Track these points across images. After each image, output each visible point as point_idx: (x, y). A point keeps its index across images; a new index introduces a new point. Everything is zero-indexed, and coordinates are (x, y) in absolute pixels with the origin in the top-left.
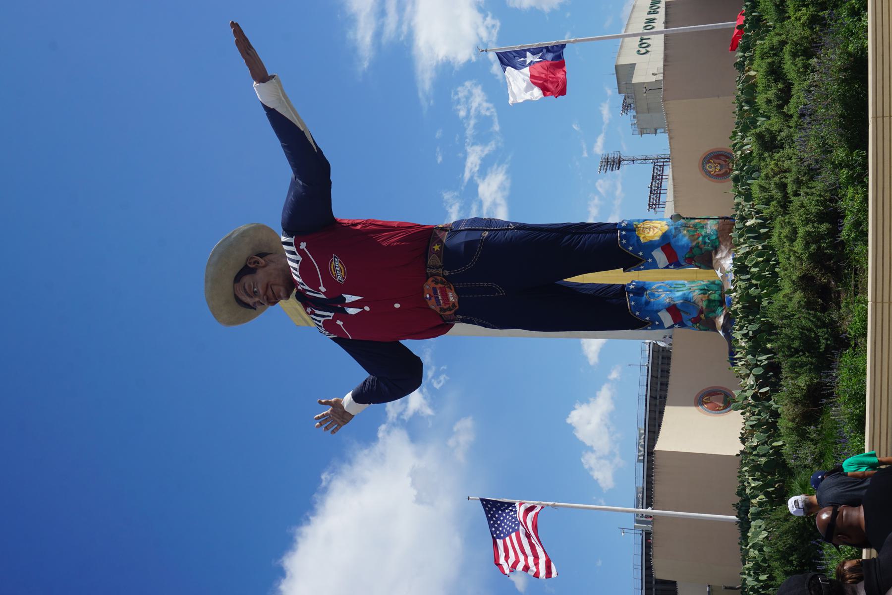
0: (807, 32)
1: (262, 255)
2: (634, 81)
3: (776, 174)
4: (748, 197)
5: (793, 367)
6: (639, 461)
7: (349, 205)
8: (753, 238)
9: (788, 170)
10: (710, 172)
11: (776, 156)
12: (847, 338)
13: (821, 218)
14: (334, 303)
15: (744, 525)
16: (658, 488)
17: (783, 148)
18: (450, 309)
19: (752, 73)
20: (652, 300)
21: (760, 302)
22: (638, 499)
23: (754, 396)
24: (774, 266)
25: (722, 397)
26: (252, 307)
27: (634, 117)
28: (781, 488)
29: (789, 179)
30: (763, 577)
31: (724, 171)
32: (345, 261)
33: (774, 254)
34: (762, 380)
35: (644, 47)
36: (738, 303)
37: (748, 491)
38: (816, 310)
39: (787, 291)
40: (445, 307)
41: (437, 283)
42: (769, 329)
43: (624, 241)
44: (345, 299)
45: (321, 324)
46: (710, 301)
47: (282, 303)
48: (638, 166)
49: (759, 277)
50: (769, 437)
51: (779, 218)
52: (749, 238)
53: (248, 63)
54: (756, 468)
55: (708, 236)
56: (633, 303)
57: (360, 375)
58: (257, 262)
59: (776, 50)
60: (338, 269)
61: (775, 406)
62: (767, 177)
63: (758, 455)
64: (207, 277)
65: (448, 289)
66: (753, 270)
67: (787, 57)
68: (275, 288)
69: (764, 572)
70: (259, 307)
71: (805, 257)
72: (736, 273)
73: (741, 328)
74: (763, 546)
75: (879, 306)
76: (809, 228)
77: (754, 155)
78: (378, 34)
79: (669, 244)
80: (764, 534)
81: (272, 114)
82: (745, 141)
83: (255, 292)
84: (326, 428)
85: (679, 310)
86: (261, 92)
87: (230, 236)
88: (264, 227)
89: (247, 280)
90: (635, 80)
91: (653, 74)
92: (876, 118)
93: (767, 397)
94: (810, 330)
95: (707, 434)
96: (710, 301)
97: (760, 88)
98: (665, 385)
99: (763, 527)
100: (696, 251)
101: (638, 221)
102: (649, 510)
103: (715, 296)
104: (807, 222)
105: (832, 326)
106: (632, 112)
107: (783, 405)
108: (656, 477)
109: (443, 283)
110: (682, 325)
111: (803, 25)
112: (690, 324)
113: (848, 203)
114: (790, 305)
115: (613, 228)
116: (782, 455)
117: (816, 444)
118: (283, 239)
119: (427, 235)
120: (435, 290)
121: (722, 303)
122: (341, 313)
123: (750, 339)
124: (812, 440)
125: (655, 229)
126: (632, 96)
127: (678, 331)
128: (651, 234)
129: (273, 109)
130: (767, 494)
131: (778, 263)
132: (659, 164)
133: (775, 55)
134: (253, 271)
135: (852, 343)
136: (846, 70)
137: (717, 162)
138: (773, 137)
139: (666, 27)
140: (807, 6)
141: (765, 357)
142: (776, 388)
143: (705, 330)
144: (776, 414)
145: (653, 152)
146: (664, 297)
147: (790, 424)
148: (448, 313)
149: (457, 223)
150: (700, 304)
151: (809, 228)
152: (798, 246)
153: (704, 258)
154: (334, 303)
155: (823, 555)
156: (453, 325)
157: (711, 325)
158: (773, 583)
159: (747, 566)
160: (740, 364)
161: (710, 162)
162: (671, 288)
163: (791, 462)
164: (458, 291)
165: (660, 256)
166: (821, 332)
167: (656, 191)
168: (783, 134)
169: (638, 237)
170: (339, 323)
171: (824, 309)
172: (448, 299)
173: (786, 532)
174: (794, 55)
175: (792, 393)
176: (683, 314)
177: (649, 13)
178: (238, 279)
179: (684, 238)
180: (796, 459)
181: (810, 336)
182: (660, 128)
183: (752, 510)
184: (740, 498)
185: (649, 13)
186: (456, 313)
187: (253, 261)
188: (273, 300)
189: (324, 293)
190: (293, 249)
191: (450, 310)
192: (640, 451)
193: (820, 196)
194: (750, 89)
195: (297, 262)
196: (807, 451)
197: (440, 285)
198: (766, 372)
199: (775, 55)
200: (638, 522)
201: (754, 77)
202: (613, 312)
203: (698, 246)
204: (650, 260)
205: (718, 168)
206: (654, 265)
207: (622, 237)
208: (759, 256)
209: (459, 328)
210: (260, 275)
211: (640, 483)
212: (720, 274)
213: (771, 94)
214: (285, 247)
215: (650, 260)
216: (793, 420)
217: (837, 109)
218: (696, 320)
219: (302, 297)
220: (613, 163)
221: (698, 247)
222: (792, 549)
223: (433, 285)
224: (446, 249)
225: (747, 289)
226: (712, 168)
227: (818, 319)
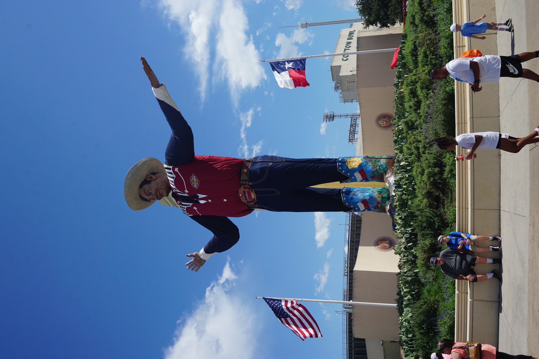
0: (428, 77)
1: (154, 174)
3: (414, 142)
4: (401, 152)
5: (423, 235)
6: (345, 275)
7: (202, 149)
8: (404, 171)
9: (420, 141)
11: (415, 133)
12: (447, 223)
13: (436, 165)
14: (193, 198)
15: (400, 311)
16: (355, 290)
17: (417, 129)
18: (252, 202)
19: (402, 90)
21: (407, 202)
22: (344, 295)
23: (405, 248)
24: (414, 185)
25: (388, 241)
26: (146, 200)
27: (341, 93)
28: (418, 292)
29: (421, 145)
30: (410, 336)
32: (198, 177)
33: (414, 179)
34: (408, 240)
36: (397, 202)
37: (402, 293)
38: (433, 208)
39: (420, 198)
41: (245, 189)
42: (412, 216)
46: (383, 197)
48: (343, 119)
49: (407, 190)
50: (412, 268)
51: (416, 164)
52: (402, 171)
53: (150, 78)
54: (406, 282)
55: (381, 166)
57: (208, 235)
59: (414, 83)
60: (195, 181)
61: (415, 252)
62: (410, 143)
63: (407, 276)
66: (404, 187)
67: (419, 89)
68: (161, 191)
69: (410, 333)
70: (152, 201)
71: (428, 183)
72: (396, 187)
73: (399, 215)
74: (410, 320)
75: (461, 209)
76: (430, 170)
77: (404, 131)
79: (362, 170)
80: (410, 315)
81: (162, 104)
82: (400, 123)
83: (150, 193)
84: (193, 269)
85: (367, 202)
88: (155, 159)
89: (146, 187)
92: (458, 123)
93: (411, 248)
94: (431, 218)
95: (379, 261)
96: (383, 197)
97: (406, 100)
98: (359, 235)
99: (410, 311)
100: (376, 173)
101: (347, 158)
102: (351, 301)
103: (385, 195)
104: (429, 167)
105: (441, 217)
107: (418, 251)
108: (355, 284)
109: (248, 188)
110: (369, 210)
111: (426, 74)
112: (373, 209)
113: (447, 159)
114: (422, 205)
115: (335, 161)
116: (418, 277)
117: (434, 272)
118: (165, 166)
119: (240, 164)
120: (244, 192)
121: (388, 198)
123: (403, 220)
124: (432, 270)
125: (355, 163)
126: (340, 82)
127: (367, 212)
128: (354, 164)
129: (163, 101)
130: (412, 295)
131: (416, 184)
132: (354, 118)
133: (413, 85)
134: (149, 182)
135: (450, 225)
136: (445, 100)
137: (385, 120)
138: (413, 124)
139: (357, 51)
140: (427, 65)
141: (410, 229)
142: (415, 244)
144: (415, 257)
145: (351, 112)
146: (360, 196)
147: (422, 262)
148: (251, 203)
149: (256, 158)
151: (430, 170)
152: (425, 178)
153: (380, 177)
154: (193, 198)
155: (437, 324)
156: (253, 210)
157: (383, 210)
158: (415, 338)
159: (402, 330)
160: (398, 232)
162: (363, 191)
163: (423, 280)
164: (256, 193)
165: (358, 175)
166: (435, 219)
167: (353, 133)
168: (417, 123)
169: (347, 166)
170: (195, 208)
171: (437, 208)
172: (251, 197)
173: (420, 314)
174: (422, 88)
175: (422, 247)
177: (348, 39)
178: (141, 186)
179: (370, 167)
180: (425, 279)
181: (430, 221)
183: (404, 303)
184: (398, 297)
185: (348, 39)
186: (255, 204)
188: (159, 197)
190: (171, 171)
192: (345, 270)
193: (435, 155)
194: (401, 98)
195: (173, 178)
198: (411, 236)
199: (413, 85)
200: (345, 308)
201: (403, 92)
202: (332, 202)
203: (376, 171)
206: (355, 180)
208: (407, 180)
209: (257, 212)
210: (153, 185)
211: (346, 287)
212: (388, 185)
213: (411, 103)
214: (166, 170)
216: (423, 260)
217: (441, 117)
218: (376, 207)
219: (175, 195)
220: (331, 118)
222: (423, 322)
223: (244, 190)
224: (249, 171)
225: (401, 195)
226: (382, 123)
227: (435, 213)
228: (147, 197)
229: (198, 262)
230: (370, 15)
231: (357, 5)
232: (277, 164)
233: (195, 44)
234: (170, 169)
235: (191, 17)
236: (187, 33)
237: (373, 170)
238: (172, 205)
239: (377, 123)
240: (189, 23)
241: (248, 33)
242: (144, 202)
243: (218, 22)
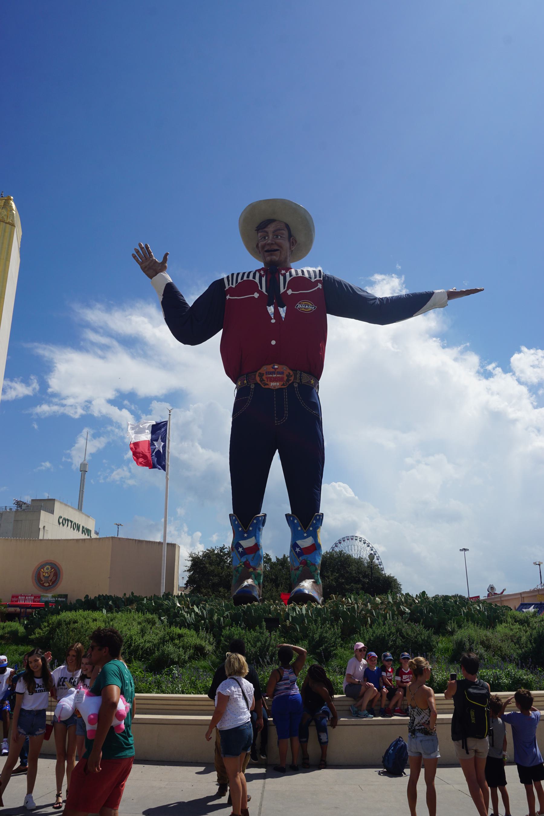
2: (42, 511)
10: (43, 568)
18: (262, 380)
31: (43, 579)
35: (64, 521)
65: (282, 383)
68: (278, 253)
78: (88, 325)
79: (316, 549)
84: (137, 252)
85: (255, 553)
89: (285, 233)
90: (42, 512)
91: (44, 527)
106: (14, 508)
109: (288, 380)
120: (282, 373)
139: (168, 544)
148: (258, 379)
161: (52, 568)
164: (279, 390)
172: (273, 381)
176: (253, 555)
177: (83, 527)
178: (287, 226)
185: (83, 527)
186: (257, 384)
187: (294, 241)
191: (261, 381)
197: (286, 378)
204: (305, 535)
205: (47, 575)
226: (47, 570)
228: (271, 229)
239: (47, 563)
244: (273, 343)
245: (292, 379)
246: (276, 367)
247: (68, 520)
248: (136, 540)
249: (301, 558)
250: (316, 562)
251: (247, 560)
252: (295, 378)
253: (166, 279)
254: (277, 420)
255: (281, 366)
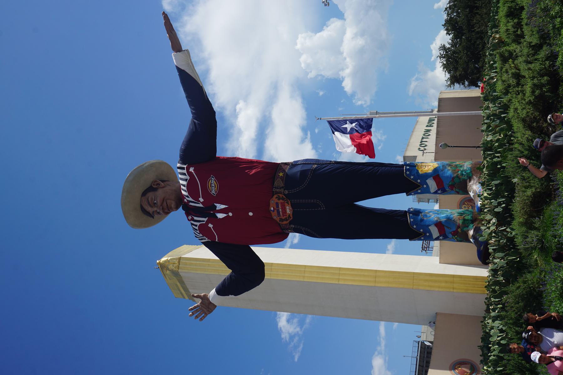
14: (208, 211)
20: (425, 219)
25: (469, 366)
26: (151, 215)
32: (218, 179)
40: (283, 218)
41: (279, 199)
43: (408, 173)
44: (216, 207)
45: (197, 228)
47: (173, 214)
55: (465, 171)
56: (412, 220)
58: (159, 184)
60: (213, 185)
64: (124, 189)
65: (286, 204)
68: (169, 201)
70: (156, 216)
79: (438, 175)
83: (155, 204)
84: (197, 317)
85: (444, 226)
86: (175, 59)
87: (143, 165)
88: (165, 163)
89: (150, 195)
100: (456, 180)
109: (283, 199)
120: (277, 204)
122: (212, 218)
128: (426, 169)
129: (184, 70)
134: (155, 190)
143: (461, 241)
146: (434, 217)
148: (285, 222)
150: (458, 221)
157: (464, 238)
161: (464, 204)
164: (293, 206)
165: (432, 184)
169: (418, 171)
170: (210, 226)
172: (286, 212)
176: (446, 228)
177: (427, 126)
178: (144, 194)
179: (449, 172)
182: (431, 199)
185: (427, 126)
186: (290, 223)
187: (156, 183)
188: (167, 211)
189: (202, 203)
191: (287, 220)
195: (186, 180)
196: (533, 236)
197: (281, 201)
204: (425, 186)
207: (407, 170)
210: (160, 193)
215: (425, 186)
218: (455, 233)
221: (458, 177)
223: (276, 200)
224: (287, 175)
228: (150, 209)
229: (207, 307)
230: (456, 69)
231: (440, 58)
232: (324, 166)
233: (240, 139)
234: (183, 168)
235: (238, 107)
236: (232, 126)
237: (452, 176)
238: (187, 298)
240: (235, 115)
241: (304, 129)
242: (145, 217)
243: (270, 113)
244: (251, 214)
245: (281, 195)
246: (272, 209)
247: (422, 142)
248: (436, 137)
249: (447, 190)
250: (451, 176)
251: (451, 233)
252: (281, 193)
253: (214, 295)
254: (321, 208)
255: (271, 205)
